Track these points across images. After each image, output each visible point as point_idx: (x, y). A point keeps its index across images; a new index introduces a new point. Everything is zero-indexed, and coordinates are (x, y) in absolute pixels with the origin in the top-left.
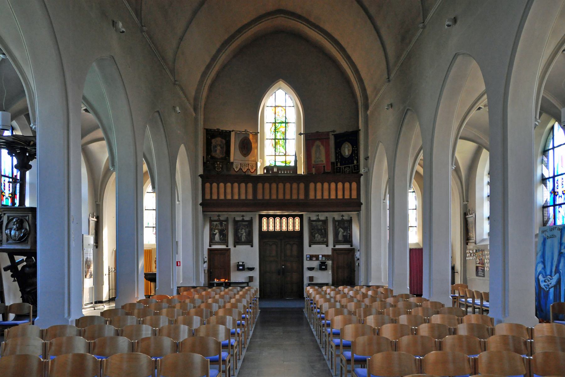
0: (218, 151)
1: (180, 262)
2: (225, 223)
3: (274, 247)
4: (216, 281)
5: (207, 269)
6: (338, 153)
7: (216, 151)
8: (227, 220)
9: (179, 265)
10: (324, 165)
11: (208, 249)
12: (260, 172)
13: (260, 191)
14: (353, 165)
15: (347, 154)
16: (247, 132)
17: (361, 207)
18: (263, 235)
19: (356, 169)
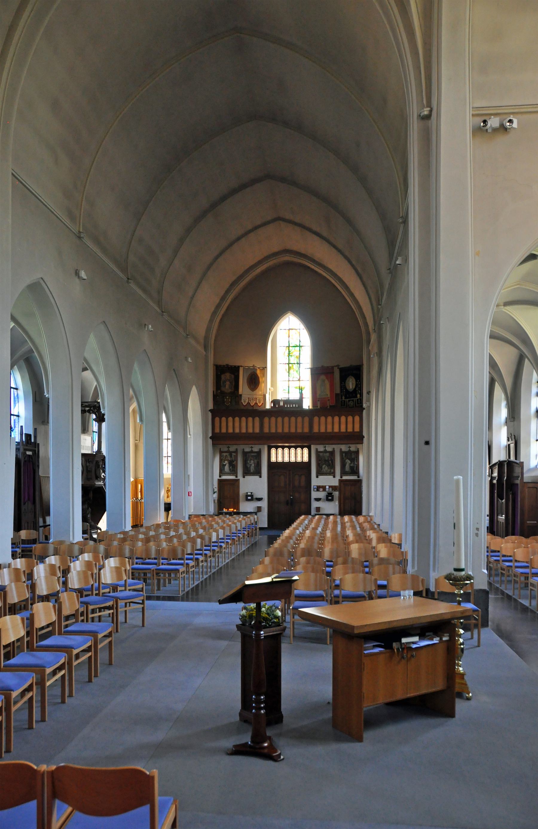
0: (227, 387)
1: (191, 492)
2: (235, 454)
3: (282, 477)
4: (225, 510)
5: (216, 499)
6: (343, 387)
7: (225, 386)
8: (236, 451)
9: (190, 495)
10: (329, 399)
11: (218, 479)
12: (268, 406)
13: (266, 425)
14: (356, 399)
15: (351, 387)
16: (255, 367)
17: (363, 440)
18: (273, 466)
19: (359, 402)
